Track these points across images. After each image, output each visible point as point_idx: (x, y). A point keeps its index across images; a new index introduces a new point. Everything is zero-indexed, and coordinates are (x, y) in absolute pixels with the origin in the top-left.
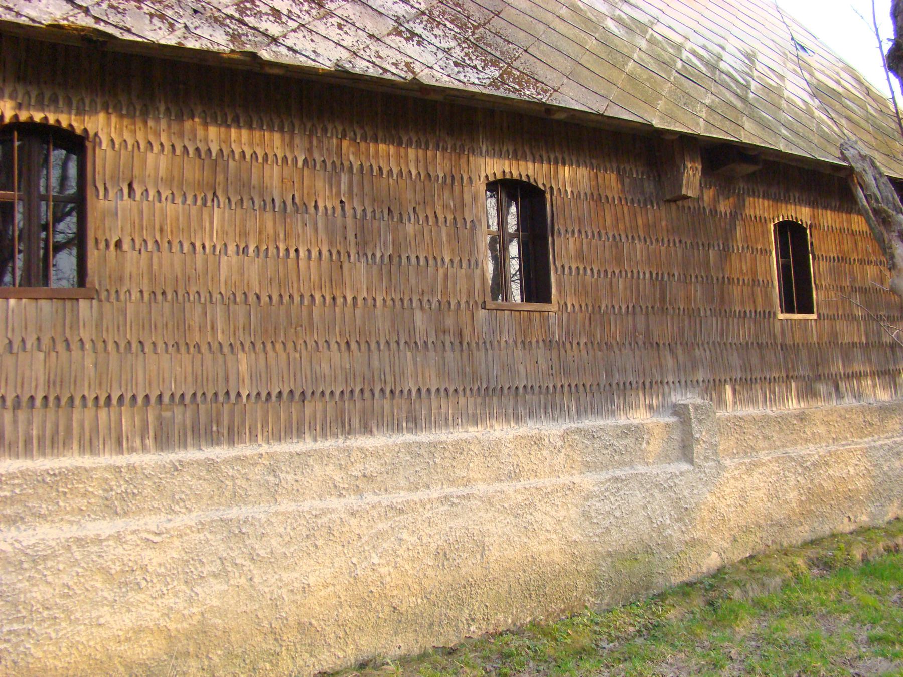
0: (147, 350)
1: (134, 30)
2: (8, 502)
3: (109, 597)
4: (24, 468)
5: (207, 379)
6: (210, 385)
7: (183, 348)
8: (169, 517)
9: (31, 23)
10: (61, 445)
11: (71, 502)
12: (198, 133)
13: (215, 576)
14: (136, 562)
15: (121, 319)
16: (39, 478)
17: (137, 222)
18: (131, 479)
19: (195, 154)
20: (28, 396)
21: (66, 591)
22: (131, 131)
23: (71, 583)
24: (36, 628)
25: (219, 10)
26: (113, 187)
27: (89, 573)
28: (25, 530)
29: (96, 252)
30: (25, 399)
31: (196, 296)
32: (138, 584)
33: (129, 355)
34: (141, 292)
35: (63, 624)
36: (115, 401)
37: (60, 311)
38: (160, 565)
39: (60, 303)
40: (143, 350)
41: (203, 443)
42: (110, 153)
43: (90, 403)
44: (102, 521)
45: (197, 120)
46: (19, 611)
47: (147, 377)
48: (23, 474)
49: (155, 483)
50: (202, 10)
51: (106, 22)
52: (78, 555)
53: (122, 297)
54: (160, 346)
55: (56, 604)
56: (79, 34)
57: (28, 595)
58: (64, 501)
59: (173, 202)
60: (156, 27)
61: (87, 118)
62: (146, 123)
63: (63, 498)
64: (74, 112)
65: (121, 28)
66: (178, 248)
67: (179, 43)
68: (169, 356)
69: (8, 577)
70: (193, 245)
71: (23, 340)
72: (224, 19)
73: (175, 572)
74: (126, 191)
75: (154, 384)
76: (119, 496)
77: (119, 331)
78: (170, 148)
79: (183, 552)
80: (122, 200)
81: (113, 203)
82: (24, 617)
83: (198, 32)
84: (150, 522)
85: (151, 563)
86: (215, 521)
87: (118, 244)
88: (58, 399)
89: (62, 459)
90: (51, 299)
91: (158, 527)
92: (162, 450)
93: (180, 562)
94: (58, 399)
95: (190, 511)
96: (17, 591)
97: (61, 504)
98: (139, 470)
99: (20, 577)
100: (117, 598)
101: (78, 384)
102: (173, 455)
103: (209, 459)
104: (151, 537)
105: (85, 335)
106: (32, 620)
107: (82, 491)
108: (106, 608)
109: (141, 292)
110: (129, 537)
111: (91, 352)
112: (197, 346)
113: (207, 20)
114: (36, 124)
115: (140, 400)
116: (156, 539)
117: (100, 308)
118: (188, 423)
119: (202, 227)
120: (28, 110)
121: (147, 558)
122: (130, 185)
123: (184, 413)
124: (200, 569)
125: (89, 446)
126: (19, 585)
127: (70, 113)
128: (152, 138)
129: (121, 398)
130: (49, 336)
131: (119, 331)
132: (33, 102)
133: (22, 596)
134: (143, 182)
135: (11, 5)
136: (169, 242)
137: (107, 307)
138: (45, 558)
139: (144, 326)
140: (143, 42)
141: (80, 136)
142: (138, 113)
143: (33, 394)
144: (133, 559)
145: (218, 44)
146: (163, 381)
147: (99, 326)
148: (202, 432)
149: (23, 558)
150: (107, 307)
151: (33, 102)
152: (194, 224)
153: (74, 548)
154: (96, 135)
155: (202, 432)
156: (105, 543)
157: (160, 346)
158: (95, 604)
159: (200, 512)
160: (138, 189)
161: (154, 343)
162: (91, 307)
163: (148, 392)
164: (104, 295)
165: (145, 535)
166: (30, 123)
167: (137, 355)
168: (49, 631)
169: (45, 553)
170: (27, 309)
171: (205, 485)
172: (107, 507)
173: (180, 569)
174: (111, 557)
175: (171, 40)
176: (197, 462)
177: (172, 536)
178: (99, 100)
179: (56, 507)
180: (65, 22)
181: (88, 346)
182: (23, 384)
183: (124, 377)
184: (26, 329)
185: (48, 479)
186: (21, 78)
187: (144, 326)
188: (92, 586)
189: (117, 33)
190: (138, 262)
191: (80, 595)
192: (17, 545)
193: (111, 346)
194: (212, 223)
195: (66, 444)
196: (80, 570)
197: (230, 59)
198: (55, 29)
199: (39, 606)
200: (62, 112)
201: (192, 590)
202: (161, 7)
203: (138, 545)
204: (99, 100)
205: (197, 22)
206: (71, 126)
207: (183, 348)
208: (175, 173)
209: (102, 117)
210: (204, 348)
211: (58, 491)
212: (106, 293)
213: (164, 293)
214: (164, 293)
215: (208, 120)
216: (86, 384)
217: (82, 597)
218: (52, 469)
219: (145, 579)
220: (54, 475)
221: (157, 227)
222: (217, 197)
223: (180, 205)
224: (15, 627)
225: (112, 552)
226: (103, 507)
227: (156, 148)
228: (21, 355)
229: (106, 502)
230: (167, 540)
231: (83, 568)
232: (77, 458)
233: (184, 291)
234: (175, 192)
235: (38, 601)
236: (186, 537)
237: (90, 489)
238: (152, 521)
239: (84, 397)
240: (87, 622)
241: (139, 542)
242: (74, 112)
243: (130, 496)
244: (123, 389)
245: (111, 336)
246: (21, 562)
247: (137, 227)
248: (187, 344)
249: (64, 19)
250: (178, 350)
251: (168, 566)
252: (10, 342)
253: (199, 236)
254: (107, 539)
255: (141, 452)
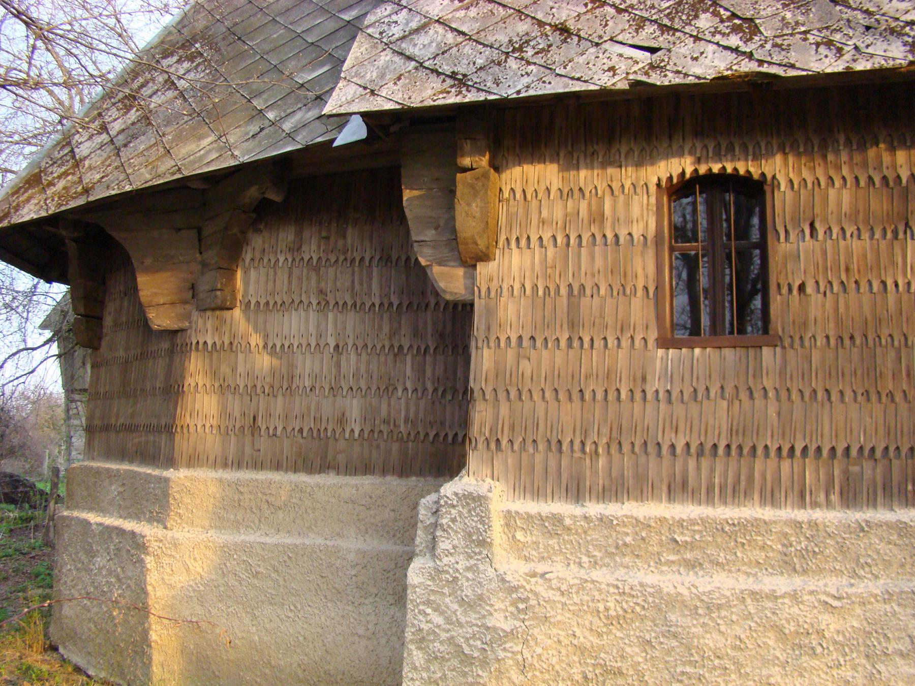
0: (833, 398)
1: (798, 65)
2: (689, 547)
3: (781, 657)
4: (704, 515)
5: (902, 431)
6: (905, 439)
7: (874, 397)
8: (852, 581)
9: (697, 81)
10: (742, 494)
11: (749, 554)
12: (884, 159)
13: (902, 655)
14: (812, 625)
15: (806, 367)
16: (719, 527)
17: (820, 263)
18: (812, 536)
19: (882, 184)
20: (712, 443)
21: (738, 643)
22: (810, 168)
23: (742, 636)
24: (707, 675)
25: (897, 19)
26: (794, 228)
27: (761, 629)
28: (703, 576)
29: (778, 297)
30: (708, 446)
31: (889, 339)
32: (813, 648)
33: (815, 404)
34: (827, 337)
35: (733, 676)
36: (798, 452)
37: (743, 360)
38: (838, 632)
39: (743, 351)
40: (829, 399)
41: (895, 503)
42: (789, 195)
43: (773, 453)
44: (779, 577)
45: (882, 146)
46: (692, 655)
47: (834, 428)
48: (703, 521)
49: (837, 543)
50: (876, 25)
51: (770, 63)
52: (752, 610)
53: (807, 344)
54: (848, 394)
55: (727, 655)
56: (744, 81)
57: (701, 641)
58: (742, 552)
59: (859, 238)
60: (822, 56)
61: (763, 162)
62: (825, 157)
63: (741, 549)
64: (750, 158)
65: (785, 66)
66: (867, 288)
67: (848, 68)
68: (857, 405)
69: (684, 620)
70: (884, 283)
71: (707, 389)
72: (904, 27)
73: (855, 643)
74: (807, 231)
75: (841, 436)
76: (798, 553)
77: (803, 378)
78: (854, 180)
79: (865, 623)
80: (804, 241)
81: (795, 245)
82: (697, 662)
83: (870, 50)
84: (830, 584)
85: (828, 629)
86: (905, 592)
87: (802, 288)
88: (740, 447)
89: (743, 509)
90: (735, 347)
91: (838, 591)
92: (848, 507)
93: (861, 633)
94: (740, 447)
95: (876, 577)
96: (691, 635)
97: (739, 554)
98: (821, 527)
99: (695, 622)
100: (789, 660)
101: (760, 433)
102: (861, 513)
103: (901, 522)
104: (830, 600)
105: (768, 383)
106: (704, 666)
107: (760, 543)
108: (777, 668)
109: (827, 337)
110: (806, 598)
111: (774, 401)
112: (891, 395)
113: (881, 34)
114: (715, 175)
115: (825, 452)
116: (836, 603)
117: (784, 356)
118: (879, 478)
119: (894, 264)
120: (707, 162)
121: (824, 623)
122: (812, 225)
123: (874, 469)
124: (884, 645)
125: (770, 497)
126: (694, 630)
127: (746, 160)
128: (832, 173)
129: (805, 450)
130: (733, 385)
131: (803, 378)
132: (711, 155)
133: (696, 640)
134: (825, 220)
135: (680, 69)
136: (856, 282)
137: (791, 353)
138: (719, 607)
139: (830, 374)
140: (807, 75)
141: (757, 181)
142: (816, 149)
143: (716, 442)
144: (808, 621)
145: (894, 59)
146: (822, 437)
147: (782, 374)
148: (895, 490)
149: (698, 604)
150: (791, 353)
151: (711, 155)
152: (884, 260)
153: (749, 601)
154: (774, 177)
155: (895, 490)
156: (780, 601)
157: (848, 394)
158: (766, 662)
159: (889, 581)
160: (820, 229)
161: (841, 392)
162: (775, 354)
163: (834, 444)
164: (787, 343)
165: (823, 598)
166: (710, 175)
167: (823, 405)
168: (718, 680)
169: (719, 602)
170: (712, 357)
171: (896, 551)
172: (786, 563)
173: (861, 640)
174: (786, 615)
175: (838, 67)
176: (886, 523)
177: (853, 603)
178: (774, 142)
179: (734, 557)
180: (729, 72)
181: (771, 394)
182: (706, 431)
183: (808, 427)
184: (710, 377)
185: (727, 528)
186: (699, 133)
187: (830, 374)
188: (764, 643)
189: (780, 71)
190: (823, 305)
191: (751, 650)
192: (693, 590)
193: (795, 395)
194: (905, 257)
195: (748, 494)
196: (753, 624)
197: (908, 72)
198: (721, 81)
199: (710, 653)
200: (739, 159)
201: (875, 667)
202: (828, 33)
203: (815, 607)
204: (774, 142)
205: (869, 39)
206: (748, 172)
207: (874, 397)
208: (861, 208)
209: (779, 158)
210: (898, 397)
211: (736, 541)
212: (789, 340)
213: (852, 338)
214: (852, 338)
215: (896, 144)
216: (769, 434)
217: (754, 652)
218: (732, 519)
219: (820, 644)
220: (734, 524)
221: (843, 268)
222: (910, 228)
223: (868, 241)
224: (688, 669)
225: (787, 610)
226: (781, 563)
227: (838, 183)
228: (705, 402)
229: (785, 558)
230: (848, 606)
231: (756, 622)
232: (758, 509)
233: (874, 335)
234: (861, 227)
235: (710, 649)
236: (870, 607)
237: (769, 543)
238: (832, 584)
239: (766, 447)
240: (756, 678)
241: (816, 604)
242: (750, 158)
243: (811, 555)
244: (807, 440)
245: (794, 385)
246: (696, 608)
247: (820, 269)
248: (878, 392)
249: (727, 70)
250: (868, 400)
251: (847, 635)
252: (695, 390)
253: (890, 272)
254: (782, 597)
255: (825, 508)
